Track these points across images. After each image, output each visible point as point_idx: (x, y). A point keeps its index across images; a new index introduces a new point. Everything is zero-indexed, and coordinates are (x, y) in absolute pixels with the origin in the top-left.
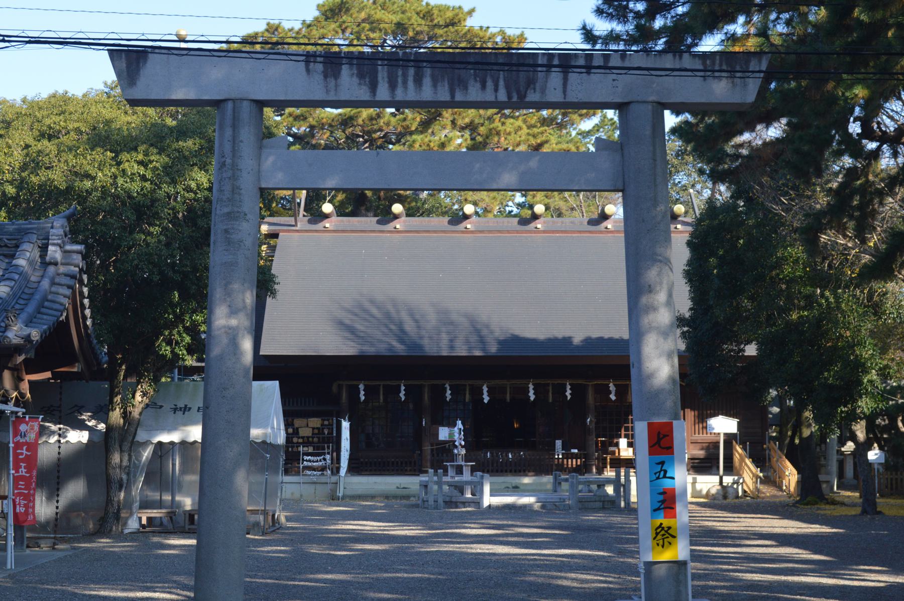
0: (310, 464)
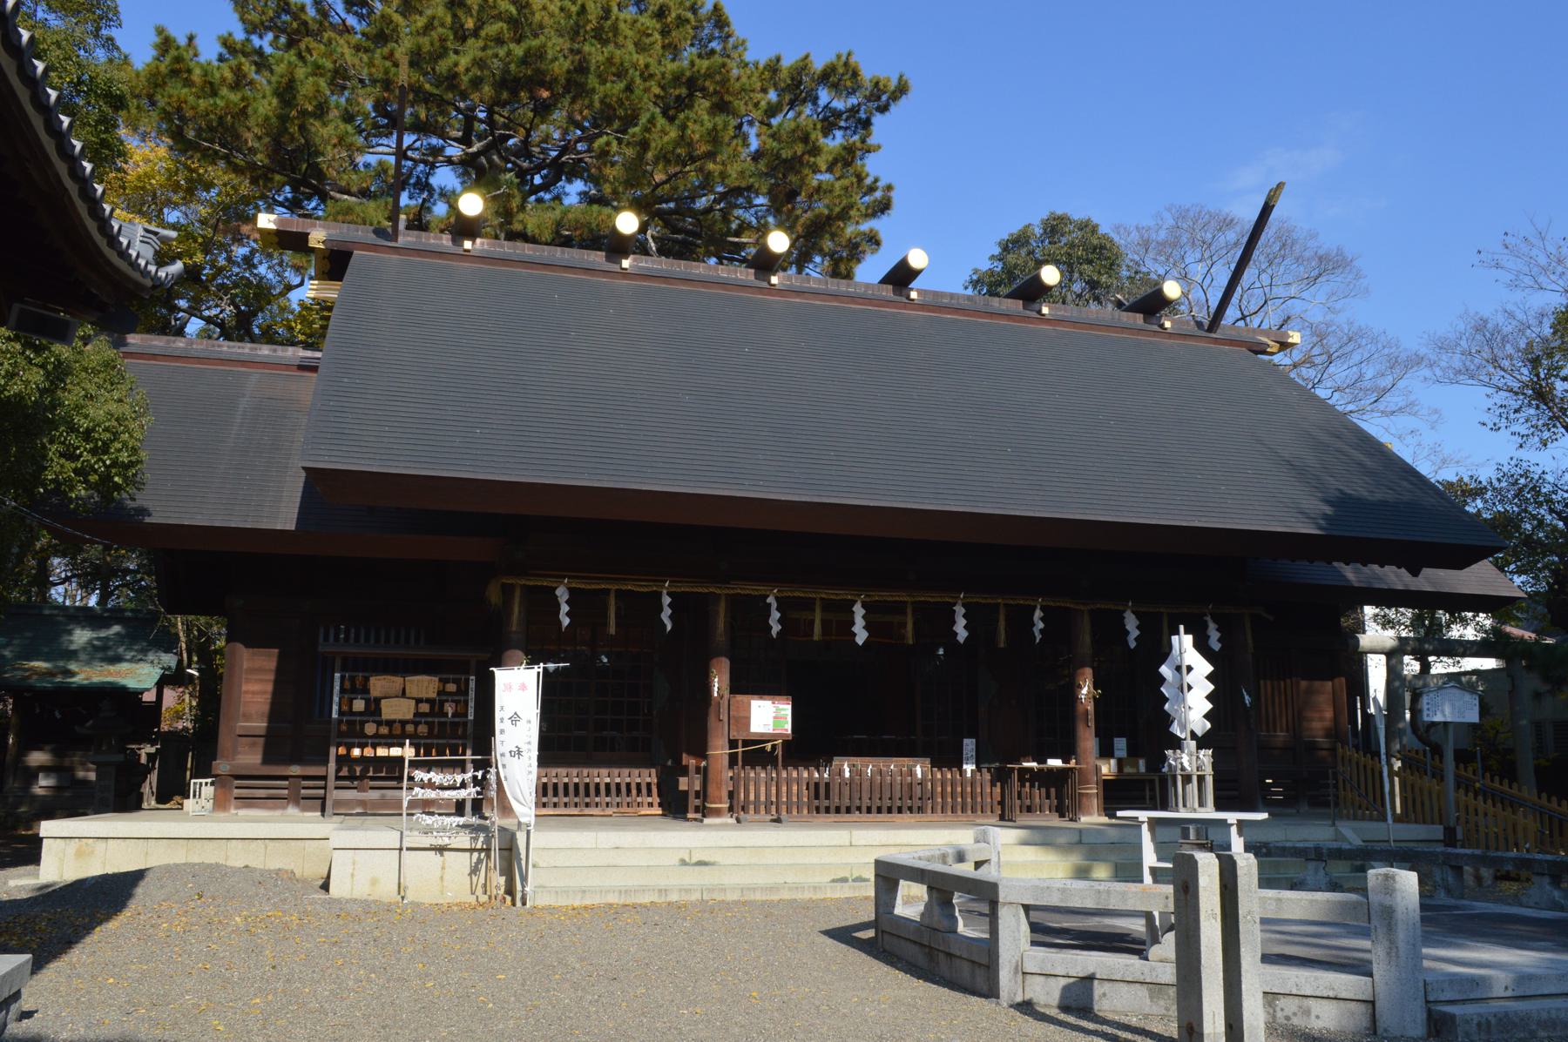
0: (431, 794)
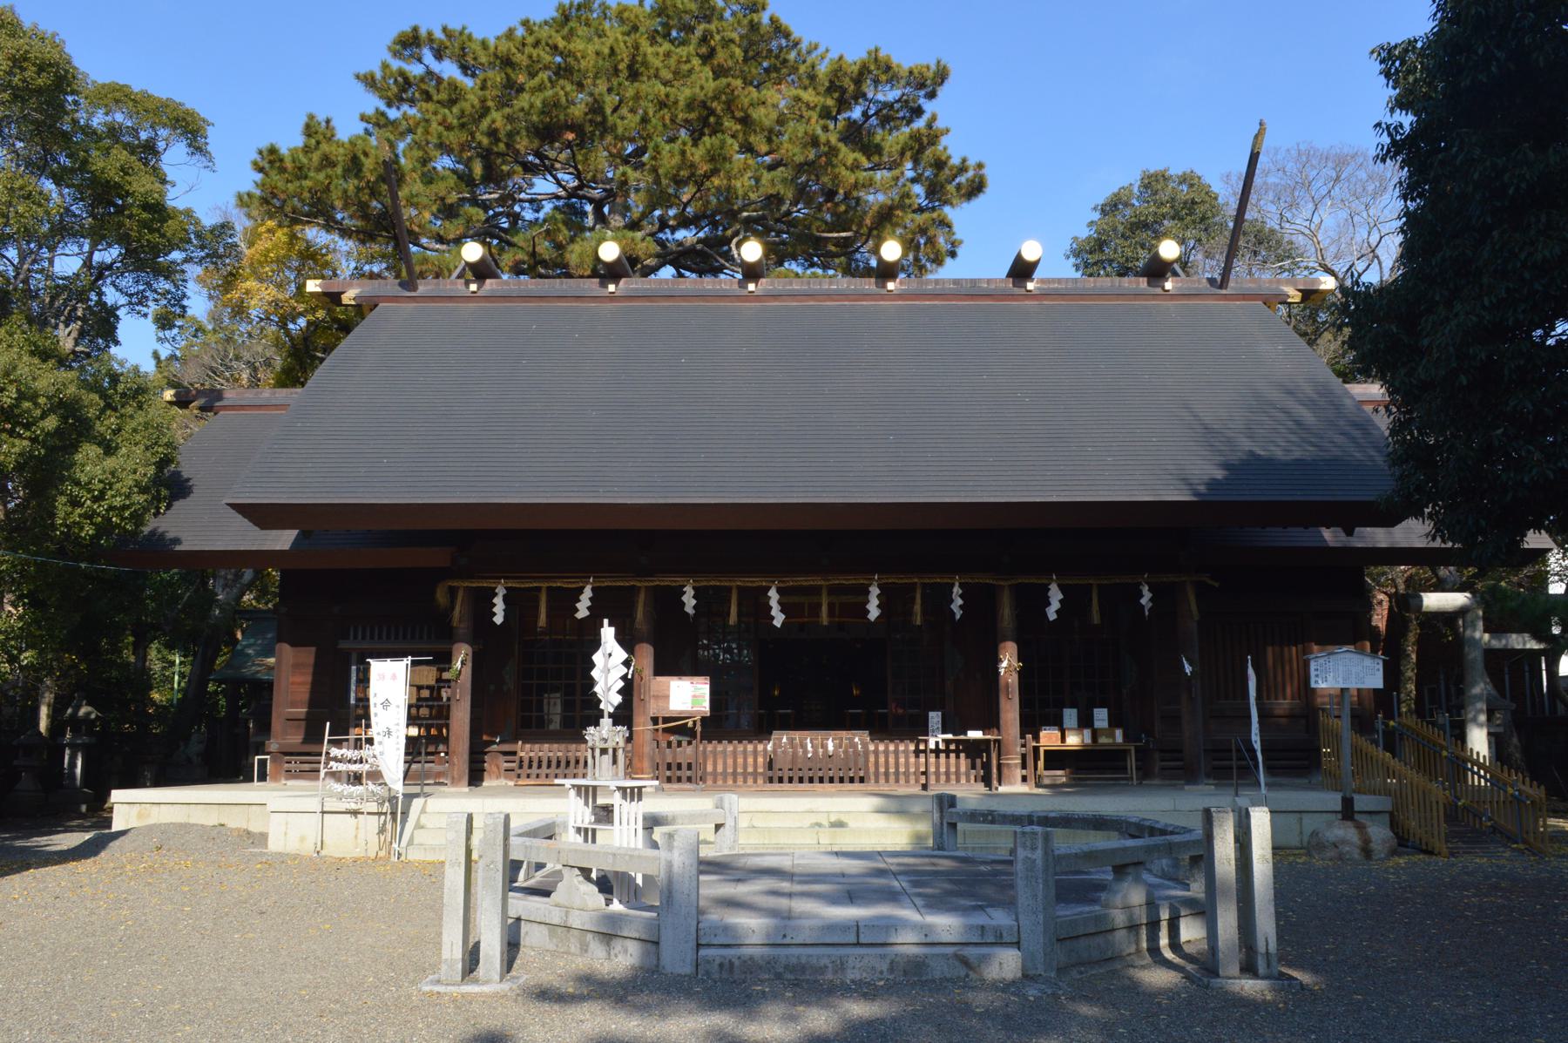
0: (342, 767)
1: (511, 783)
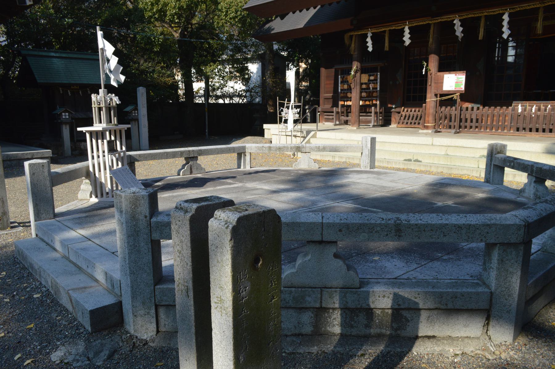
1: (355, 128)
